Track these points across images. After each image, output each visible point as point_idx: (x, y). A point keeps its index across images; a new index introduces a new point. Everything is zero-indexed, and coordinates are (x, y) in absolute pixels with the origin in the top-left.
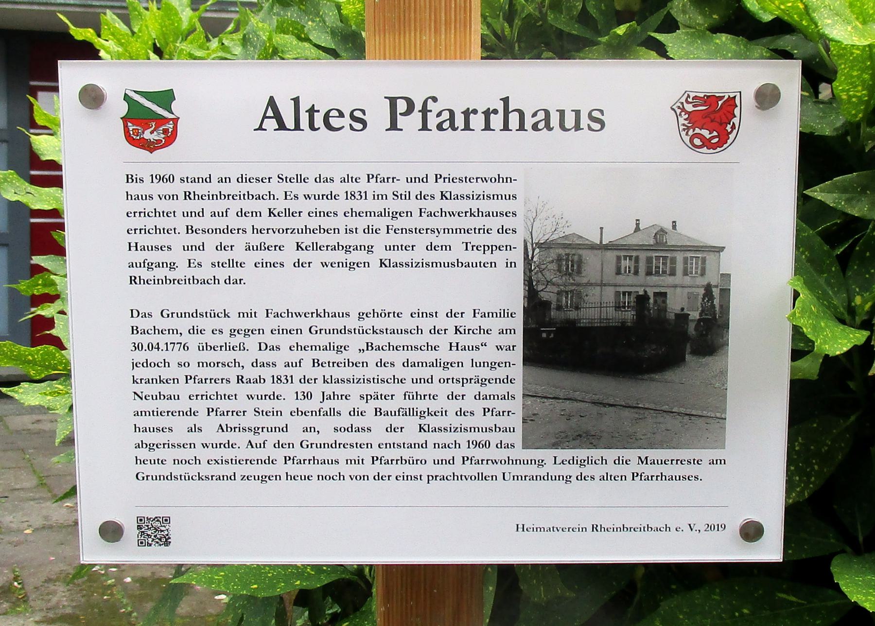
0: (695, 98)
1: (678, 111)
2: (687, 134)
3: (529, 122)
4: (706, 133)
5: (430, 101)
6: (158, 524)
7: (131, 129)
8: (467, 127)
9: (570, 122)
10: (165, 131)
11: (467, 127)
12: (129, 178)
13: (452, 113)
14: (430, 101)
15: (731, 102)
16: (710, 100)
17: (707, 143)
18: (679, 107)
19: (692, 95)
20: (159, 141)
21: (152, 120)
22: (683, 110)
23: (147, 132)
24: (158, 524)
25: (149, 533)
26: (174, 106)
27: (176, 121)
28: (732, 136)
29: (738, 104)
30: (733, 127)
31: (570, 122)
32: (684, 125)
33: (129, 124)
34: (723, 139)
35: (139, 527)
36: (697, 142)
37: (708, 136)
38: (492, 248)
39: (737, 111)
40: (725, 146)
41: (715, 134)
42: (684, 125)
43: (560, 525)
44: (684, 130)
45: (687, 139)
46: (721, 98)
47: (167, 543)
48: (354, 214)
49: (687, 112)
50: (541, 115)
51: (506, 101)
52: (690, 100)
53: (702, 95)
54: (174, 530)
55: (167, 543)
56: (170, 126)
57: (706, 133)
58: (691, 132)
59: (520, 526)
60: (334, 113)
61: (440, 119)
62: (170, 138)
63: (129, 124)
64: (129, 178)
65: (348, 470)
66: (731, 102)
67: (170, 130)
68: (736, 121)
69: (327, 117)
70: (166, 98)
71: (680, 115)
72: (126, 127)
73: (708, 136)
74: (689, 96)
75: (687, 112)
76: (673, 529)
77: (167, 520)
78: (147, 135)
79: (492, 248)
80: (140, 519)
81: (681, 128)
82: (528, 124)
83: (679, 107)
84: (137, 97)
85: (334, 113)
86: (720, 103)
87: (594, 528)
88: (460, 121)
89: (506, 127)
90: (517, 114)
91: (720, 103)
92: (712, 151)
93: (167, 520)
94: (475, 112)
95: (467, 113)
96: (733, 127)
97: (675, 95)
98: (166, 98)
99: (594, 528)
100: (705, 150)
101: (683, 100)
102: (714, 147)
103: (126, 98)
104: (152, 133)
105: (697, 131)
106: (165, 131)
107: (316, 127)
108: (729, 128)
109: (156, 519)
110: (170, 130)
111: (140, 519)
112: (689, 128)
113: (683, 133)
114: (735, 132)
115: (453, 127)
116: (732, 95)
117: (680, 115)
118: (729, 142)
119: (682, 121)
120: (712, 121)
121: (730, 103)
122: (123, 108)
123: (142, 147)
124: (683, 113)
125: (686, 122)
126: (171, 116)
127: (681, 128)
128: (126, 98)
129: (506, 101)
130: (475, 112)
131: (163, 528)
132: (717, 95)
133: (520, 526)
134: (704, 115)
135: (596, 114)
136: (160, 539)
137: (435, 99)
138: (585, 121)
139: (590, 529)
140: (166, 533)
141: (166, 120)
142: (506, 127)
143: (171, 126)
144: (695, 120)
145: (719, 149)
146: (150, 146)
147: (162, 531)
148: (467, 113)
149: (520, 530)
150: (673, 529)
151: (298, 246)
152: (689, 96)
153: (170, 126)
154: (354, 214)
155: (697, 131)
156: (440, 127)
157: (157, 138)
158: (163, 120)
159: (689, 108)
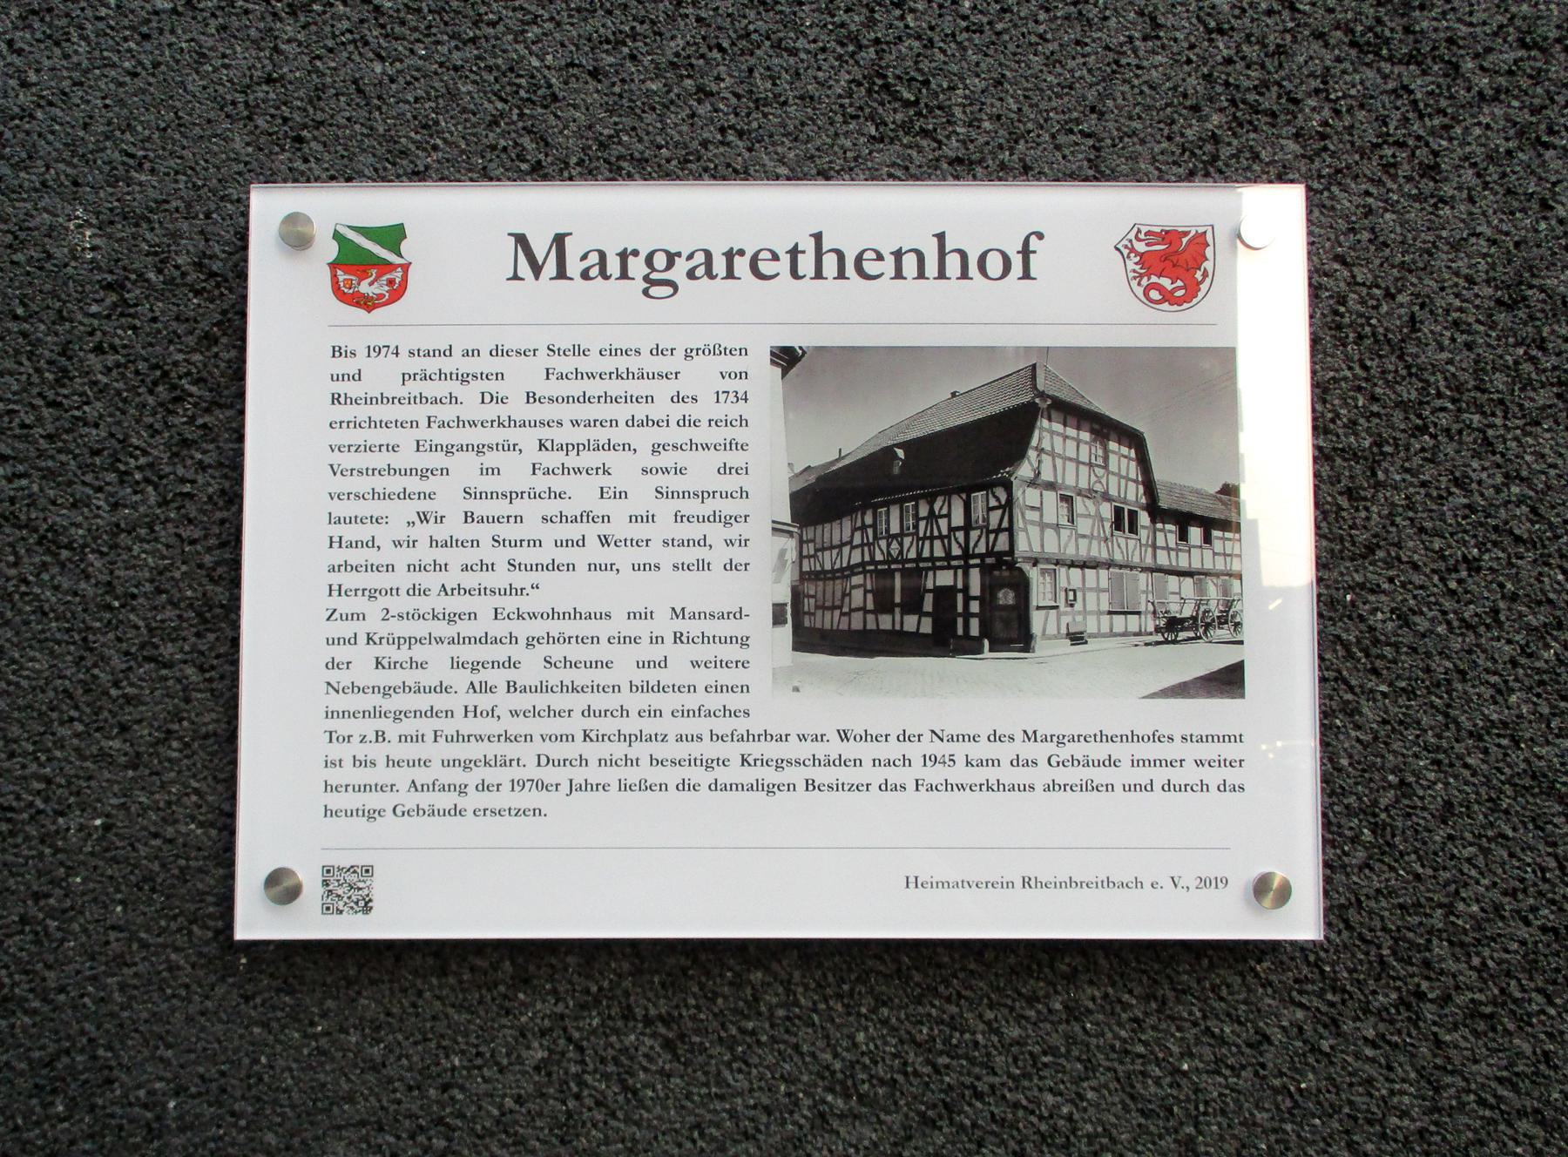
0: (1148, 233)
1: (1126, 252)
5: (1033, 238)
6: (353, 878)
7: (341, 279)
8: (730, 275)
9: (910, 263)
10: (391, 282)
11: (730, 275)
12: (337, 352)
13: (708, 255)
14: (1033, 238)
15: (1200, 241)
16: (1170, 236)
17: (1168, 297)
19: (1144, 230)
20: (381, 296)
21: (373, 266)
22: (1132, 250)
23: (365, 283)
24: (354, 878)
25: (340, 892)
26: (405, 247)
27: (406, 268)
28: (1204, 287)
30: (1205, 275)
31: (910, 263)
34: (1192, 291)
35: (326, 883)
36: (1154, 295)
37: (1170, 287)
39: (1209, 252)
43: (973, 878)
45: (1140, 291)
46: (1186, 234)
49: (1137, 254)
50: (594, 258)
51: (818, 237)
52: (1142, 236)
53: (1158, 230)
55: (367, 908)
57: (1166, 282)
58: (1145, 282)
59: (912, 880)
60: (765, 255)
61: (586, 264)
64: (337, 352)
65: (877, 776)
66: (1200, 241)
68: (1208, 265)
69: (859, 260)
70: (393, 236)
72: (334, 277)
73: (1170, 287)
74: (1139, 231)
75: (1137, 254)
76: (1147, 885)
77: (368, 870)
78: (365, 288)
80: (328, 870)
81: (1131, 275)
84: (351, 235)
85: (870, 255)
86: (1185, 240)
87: (1026, 882)
88: (719, 266)
89: (819, 275)
90: (834, 256)
92: (1175, 307)
93: (368, 870)
94: (635, 253)
95: (623, 256)
96: (1205, 275)
97: (1119, 231)
98: (393, 236)
99: (1026, 882)
100: (1166, 306)
101: (1132, 236)
102: (1179, 302)
104: (371, 284)
105: (1154, 279)
106: (391, 282)
107: (801, 273)
108: (1199, 275)
109: (352, 869)
111: (328, 870)
112: (1141, 276)
113: (1134, 283)
114: (1208, 280)
115: (604, 275)
116: (1201, 230)
118: (1200, 295)
119: (1131, 265)
121: (1200, 240)
122: (331, 251)
123: (357, 305)
125: (1137, 268)
127: (1131, 275)
128: (337, 236)
129: (818, 237)
130: (635, 253)
131: (361, 885)
133: (912, 880)
134: (1164, 257)
137: (1040, 236)
139: (1019, 883)
141: (390, 267)
142: (819, 275)
145: (1186, 305)
146: (367, 304)
148: (623, 256)
149: (912, 885)
150: (1147, 885)
151: (542, 445)
152: (1139, 231)
153: (397, 275)
155: (1154, 279)
156: (585, 275)
157: (378, 291)
158: (387, 266)
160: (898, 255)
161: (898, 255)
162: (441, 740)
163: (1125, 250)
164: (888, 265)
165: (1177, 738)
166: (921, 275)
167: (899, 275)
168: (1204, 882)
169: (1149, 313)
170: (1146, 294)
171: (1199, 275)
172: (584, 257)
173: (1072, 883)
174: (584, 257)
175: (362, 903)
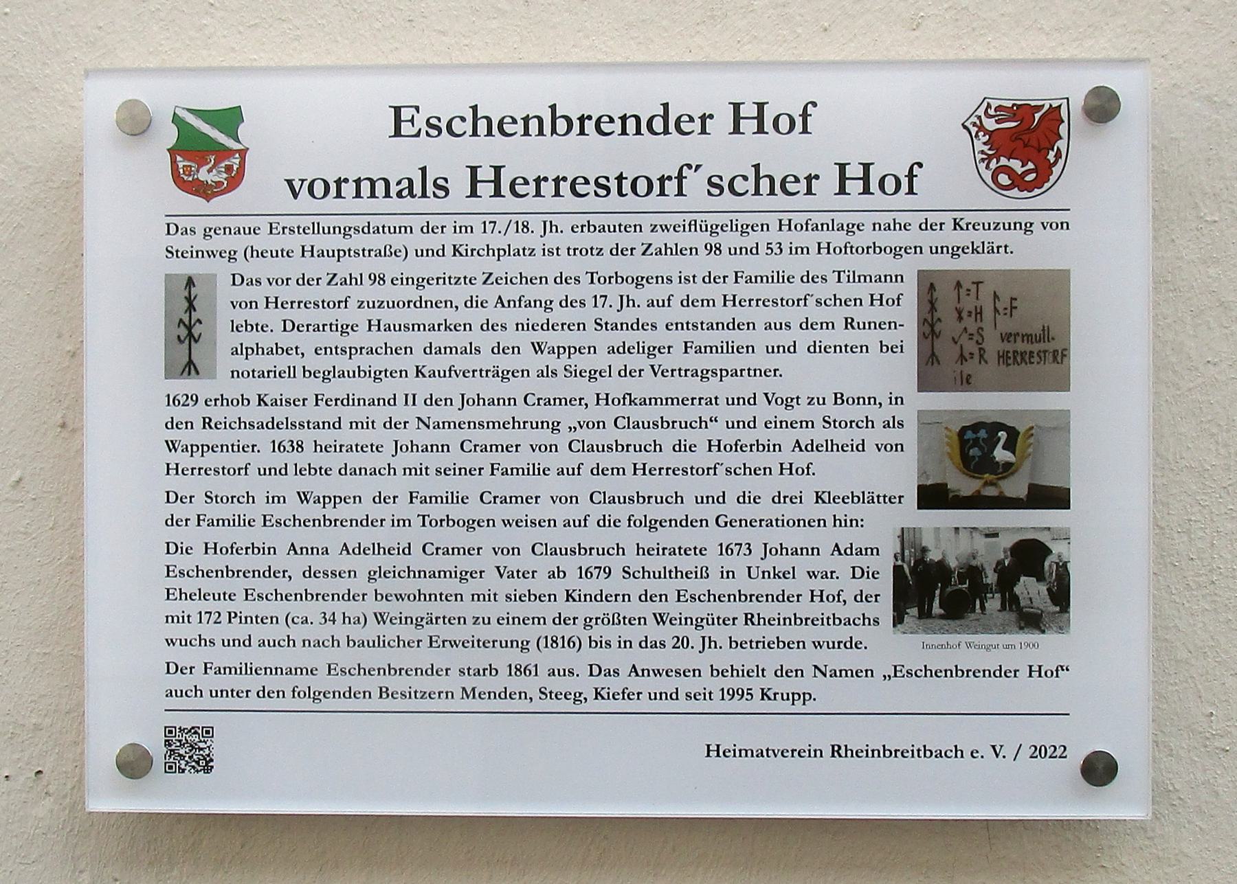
0: (998, 108)
1: (974, 130)
2: (987, 167)
3: (394, 190)
4: (1016, 165)
7: (181, 165)
9: (534, 125)
10: (229, 169)
13: (410, 181)
16: (1021, 111)
17: (1018, 182)
18: (974, 124)
19: (994, 104)
20: (219, 184)
22: (981, 127)
23: (205, 169)
25: (182, 752)
26: (241, 131)
27: (243, 153)
28: (1056, 170)
29: (1065, 118)
30: (1058, 155)
31: (534, 125)
32: (982, 152)
33: (179, 158)
35: (168, 743)
36: (1004, 179)
37: (1020, 170)
38: (471, 525)
39: (1063, 129)
40: (1047, 185)
41: (1030, 166)
42: (982, 152)
44: (983, 160)
45: (987, 175)
47: (208, 769)
48: (765, 184)
49: (986, 132)
50: (405, 183)
52: (991, 112)
53: (1009, 104)
54: (219, 748)
55: (208, 769)
56: (235, 161)
57: (1016, 165)
58: (993, 165)
62: (235, 179)
63: (179, 158)
66: (1054, 116)
67: (235, 167)
68: (1061, 144)
70: (230, 119)
71: (977, 136)
72: (174, 162)
73: (1020, 170)
74: (989, 106)
75: (986, 132)
77: (209, 732)
78: (203, 175)
79: (471, 525)
80: (169, 731)
82: (393, 193)
83: (974, 124)
86: (1037, 116)
87: (836, 751)
91: (1037, 116)
92: (1026, 194)
93: (209, 732)
96: (1058, 155)
97: (966, 106)
98: (230, 119)
99: (836, 751)
100: (1015, 192)
101: (981, 112)
102: (1029, 187)
103: (176, 119)
104: (210, 171)
105: (1003, 161)
106: (229, 169)
109: (193, 730)
110: (235, 167)
111: (169, 731)
112: (990, 158)
113: (982, 166)
114: (1061, 162)
117: (977, 136)
118: (1053, 179)
119: (979, 146)
120: (1026, 146)
122: (170, 136)
124: (981, 134)
125: (985, 148)
126: (236, 146)
128: (176, 119)
131: (202, 745)
132: (1033, 103)
135: (441, 182)
136: (198, 763)
138: (613, 185)
139: (827, 752)
140: (207, 752)
141: (229, 153)
143: (237, 161)
144: (1000, 145)
145: (1037, 191)
147: (201, 749)
150: (967, 754)
152: (989, 106)
153: (235, 161)
154: (765, 184)
155: (1003, 161)
158: (227, 153)
159: (990, 125)
160: (624, 119)
161: (624, 119)
162: (235, 621)
163: (974, 128)
164: (520, 127)
165: (218, 643)
166: (541, 133)
167: (526, 133)
168: (1039, 752)
169: (998, 201)
170: (994, 178)
171: (1051, 156)
172: (399, 183)
173: (926, 752)
174: (399, 183)
175: (203, 763)
